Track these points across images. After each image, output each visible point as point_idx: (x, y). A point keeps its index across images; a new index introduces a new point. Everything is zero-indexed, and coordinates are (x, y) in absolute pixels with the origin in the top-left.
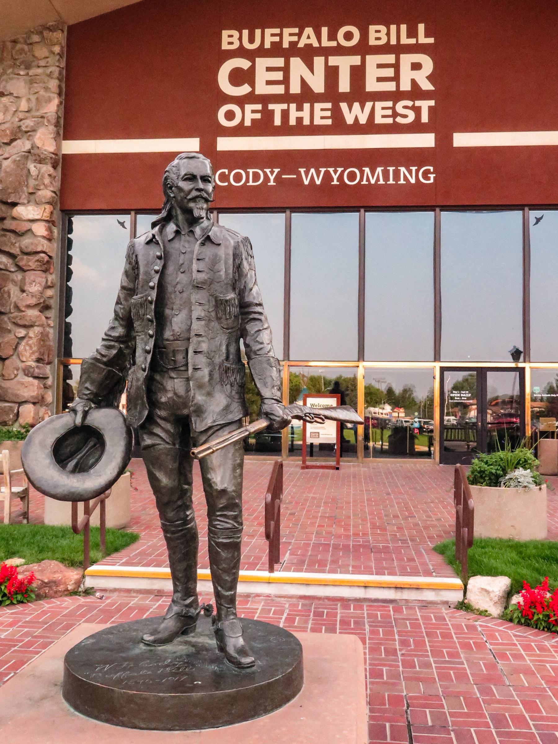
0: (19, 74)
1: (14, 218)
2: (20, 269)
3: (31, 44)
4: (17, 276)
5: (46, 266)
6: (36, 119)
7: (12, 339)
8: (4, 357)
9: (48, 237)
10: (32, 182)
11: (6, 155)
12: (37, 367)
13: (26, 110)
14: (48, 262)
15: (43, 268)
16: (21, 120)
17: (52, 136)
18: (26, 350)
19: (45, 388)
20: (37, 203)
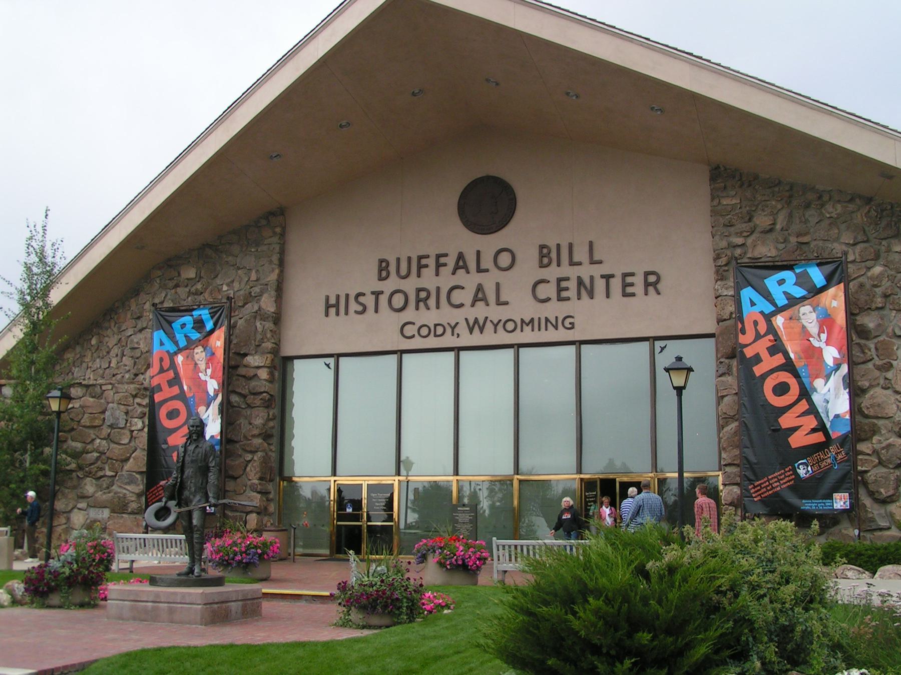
0: (251, 251)
1: (246, 366)
2: (249, 406)
3: (260, 227)
4: (246, 412)
5: (267, 403)
6: (262, 286)
7: (243, 462)
8: (236, 476)
9: (269, 380)
10: (259, 337)
11: (241, 316)
12: (260, 484)
13: (255, 279)
14: (269, 399)
15: (266, 405)
16: (252, 287)
17: (274, 299)
18: (251, 471)
19: (268, 500)
20: (263, 353)
